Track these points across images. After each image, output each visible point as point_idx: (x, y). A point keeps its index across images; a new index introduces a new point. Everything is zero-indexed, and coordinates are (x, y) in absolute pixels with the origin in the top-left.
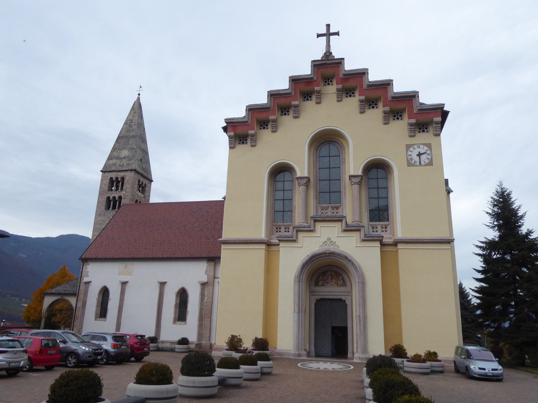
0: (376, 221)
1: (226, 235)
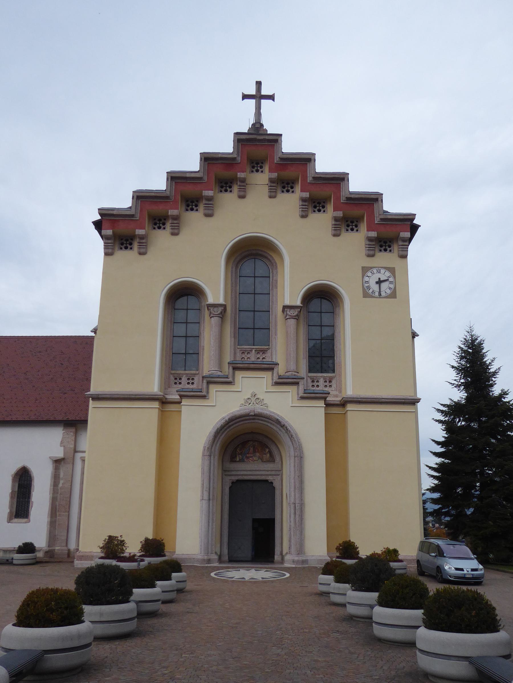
1: (96, 386)
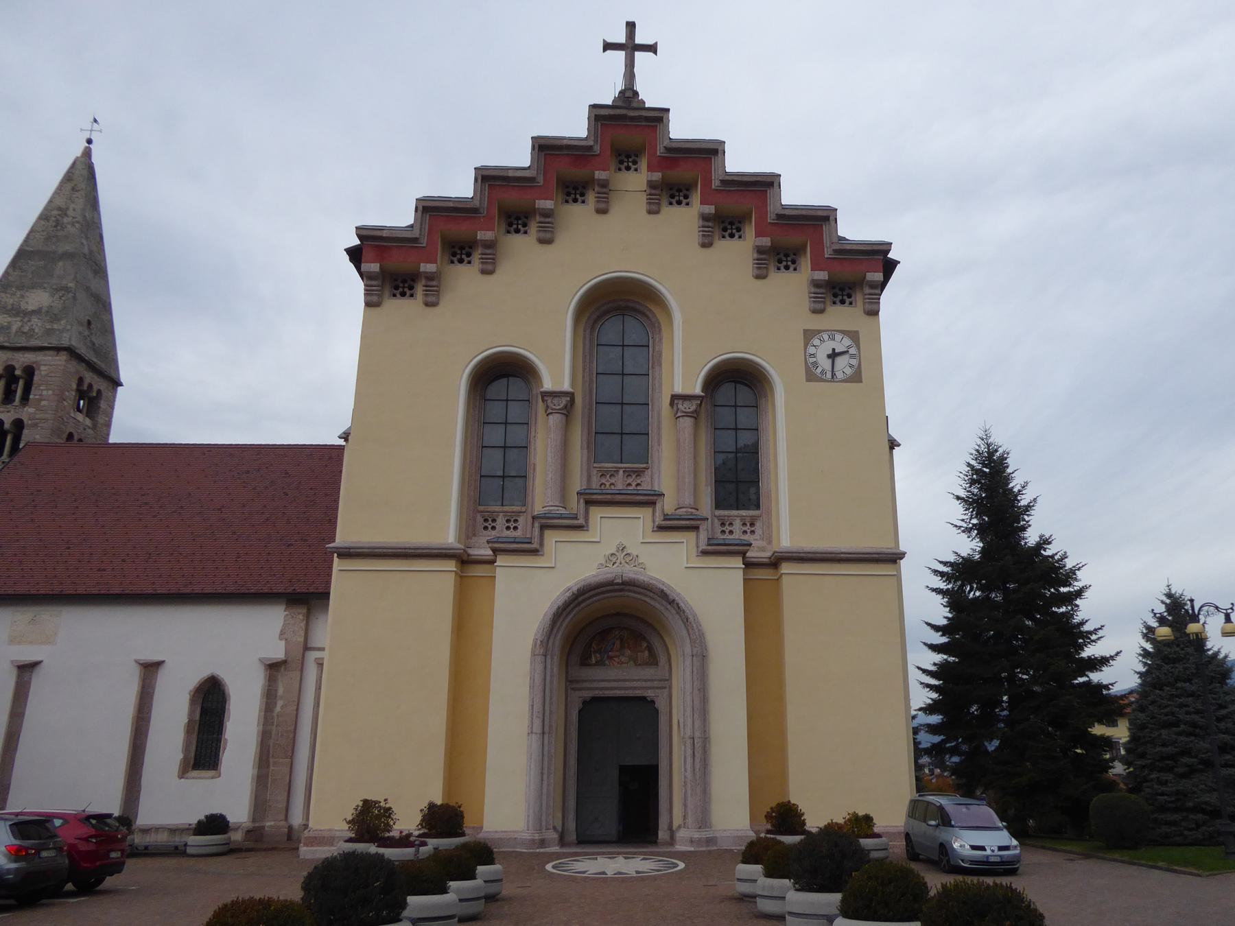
0: (730, 507)
1: (345, 535)
